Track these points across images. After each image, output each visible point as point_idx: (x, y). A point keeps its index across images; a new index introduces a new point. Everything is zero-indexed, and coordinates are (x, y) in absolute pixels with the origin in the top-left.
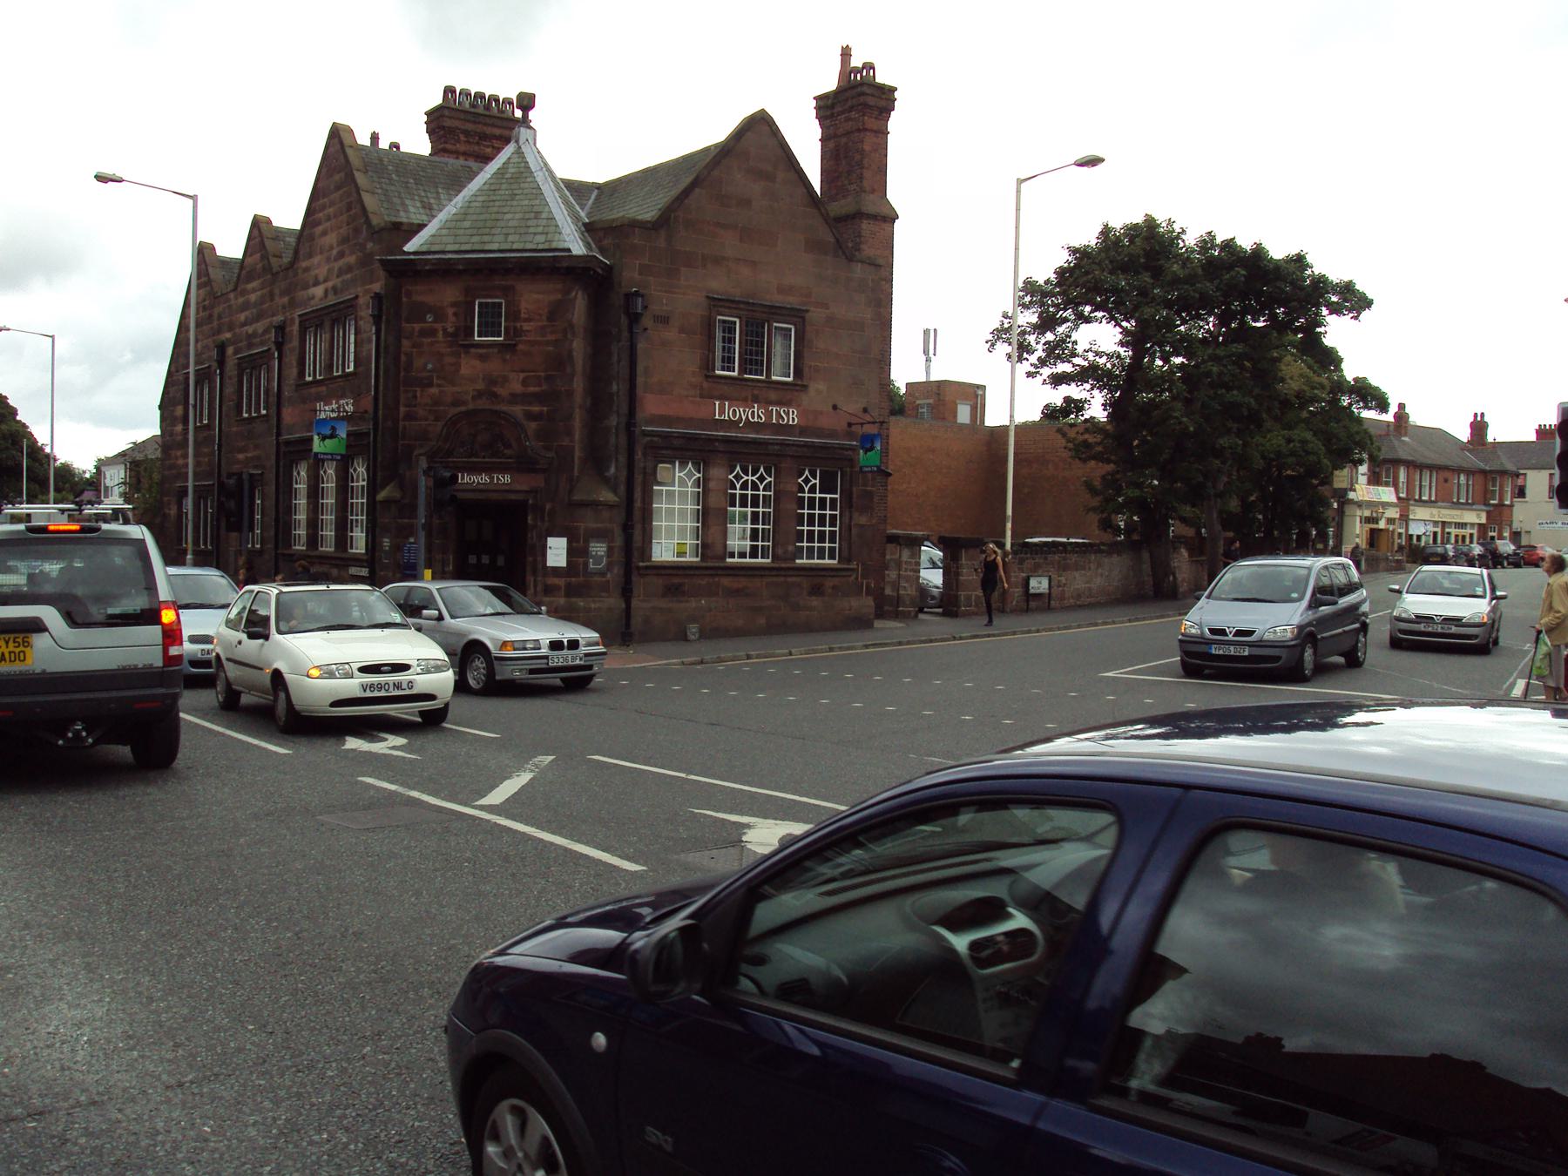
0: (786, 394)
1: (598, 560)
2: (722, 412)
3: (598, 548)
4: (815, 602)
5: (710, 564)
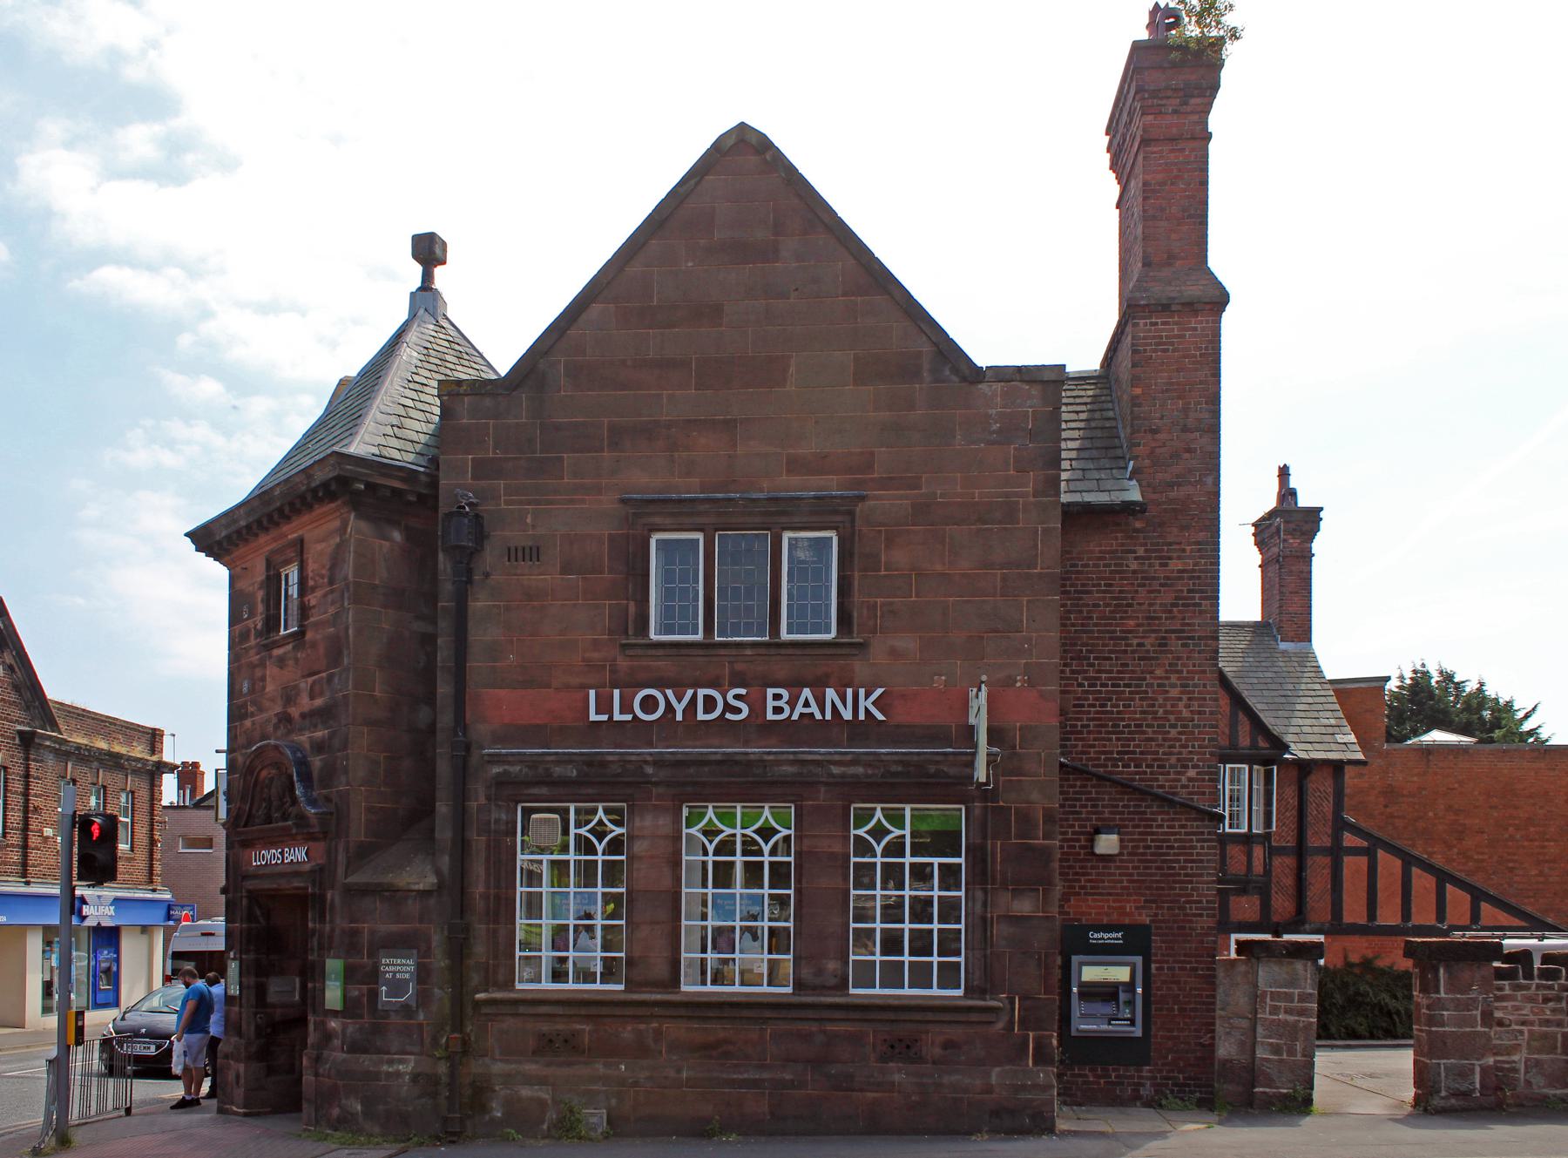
0: (811, 667)
1: (397, 987)
2: (604, 705)
3: (399, 967)
4: (899, 1075)
5: (636, 997)
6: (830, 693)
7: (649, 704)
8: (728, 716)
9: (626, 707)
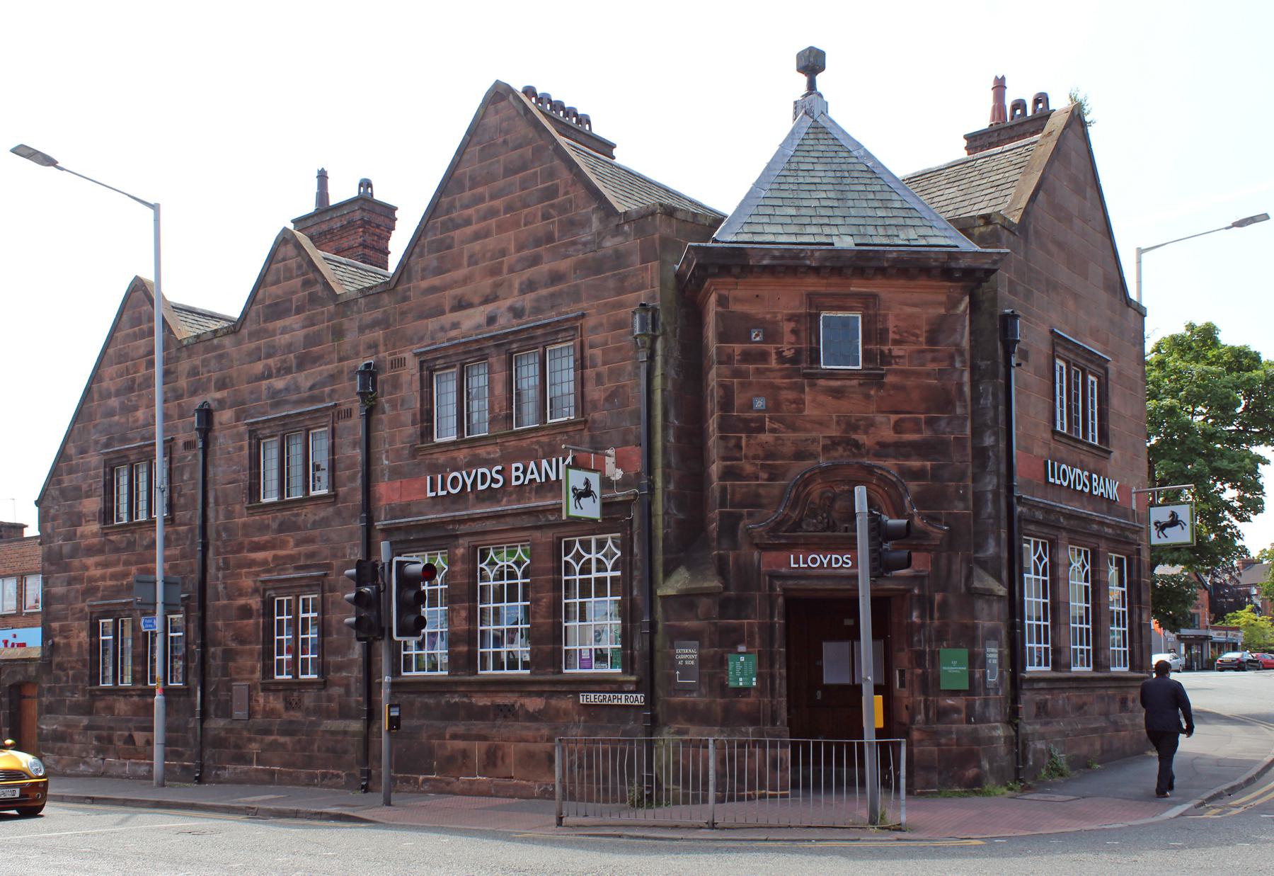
1: (686, 671)
2: (797, 561)
5: (456, 678)
6: (544, 463)
7: (814, 561)
8: (494, 486)
9: (805, 562)
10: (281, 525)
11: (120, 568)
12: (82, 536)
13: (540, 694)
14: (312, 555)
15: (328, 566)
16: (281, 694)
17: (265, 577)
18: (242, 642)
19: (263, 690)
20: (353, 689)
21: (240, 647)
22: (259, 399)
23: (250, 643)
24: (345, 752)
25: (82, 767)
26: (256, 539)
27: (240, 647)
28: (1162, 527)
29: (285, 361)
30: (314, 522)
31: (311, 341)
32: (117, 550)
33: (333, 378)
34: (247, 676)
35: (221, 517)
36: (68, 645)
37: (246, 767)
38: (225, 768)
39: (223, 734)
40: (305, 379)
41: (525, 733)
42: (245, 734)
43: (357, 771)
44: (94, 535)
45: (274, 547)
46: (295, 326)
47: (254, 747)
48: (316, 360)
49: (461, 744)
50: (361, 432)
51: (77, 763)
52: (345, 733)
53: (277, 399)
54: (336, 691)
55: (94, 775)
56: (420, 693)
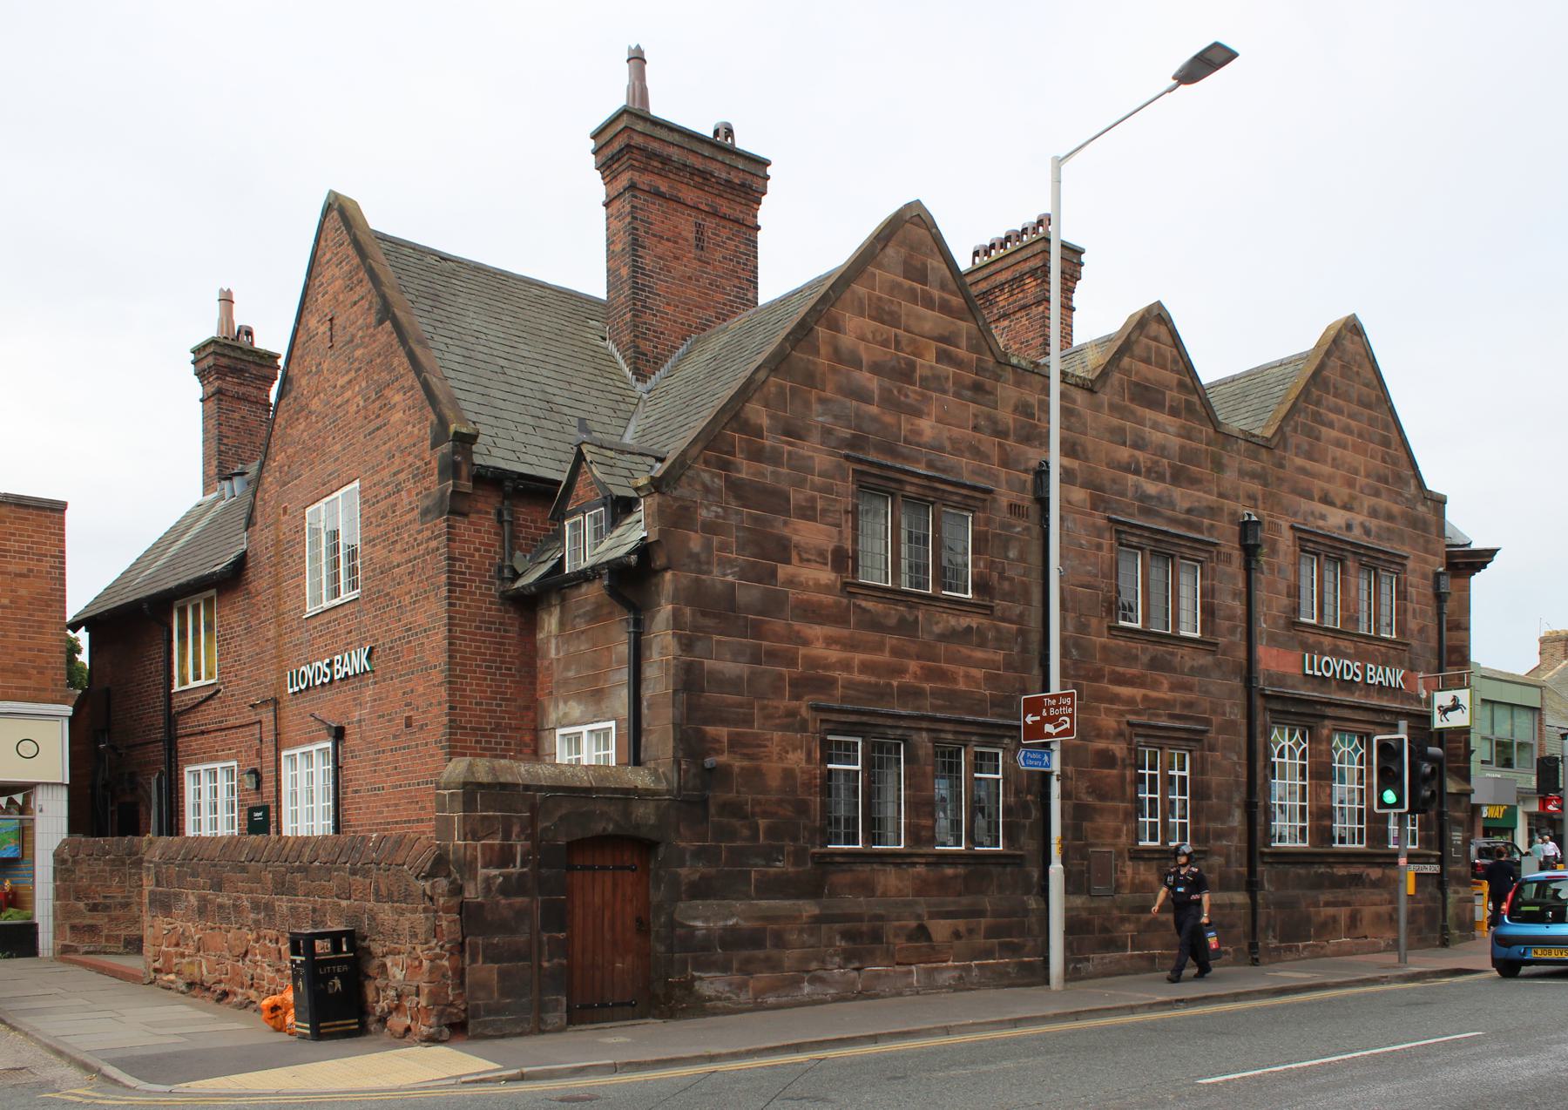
10: (1153, 659)
11: (884, 657)
12: (791, 582)
13: (1379, 865)
14: (1189, 705)
15: (1208, 722)
16: (1155, 863)
17: (1133, 718)
18: (1102, 797)
19: (1131, 859)
20: (1233, 859)
21: (1097, 803)
22: (1123, 494)
23: (1112, 799)
24: (1232, 926)
25: (807, 988)
26: (1120, 669)
27: (1097, 803)
28: (1445, 711)
29: (1156, 463)
30: (1192, 668)
31: (1187, 456)
32: (875, 624)
33: (1213, 511)
34: (1109, 841)
35: (1070, 628)
36: (757, 773)
37: (1117, 955)
38: (1087, 960)
39: (1084, 915)
40: (1184, 498)
41: (1376, 898)
42: (1116, 913)
43: (1245, 945)
44: (827, 589)
45: (1142, 685)
46: (1171, 429)
47: (1128, 929)
48: (1194, 481)
49: (1331, 911)
50: (1241, 585)
51: (796, 983)
52: (1232, 905)
53: (1147, 505)
54: (1217, 860)
55: (835, 1000)
56: (1294, 863)
